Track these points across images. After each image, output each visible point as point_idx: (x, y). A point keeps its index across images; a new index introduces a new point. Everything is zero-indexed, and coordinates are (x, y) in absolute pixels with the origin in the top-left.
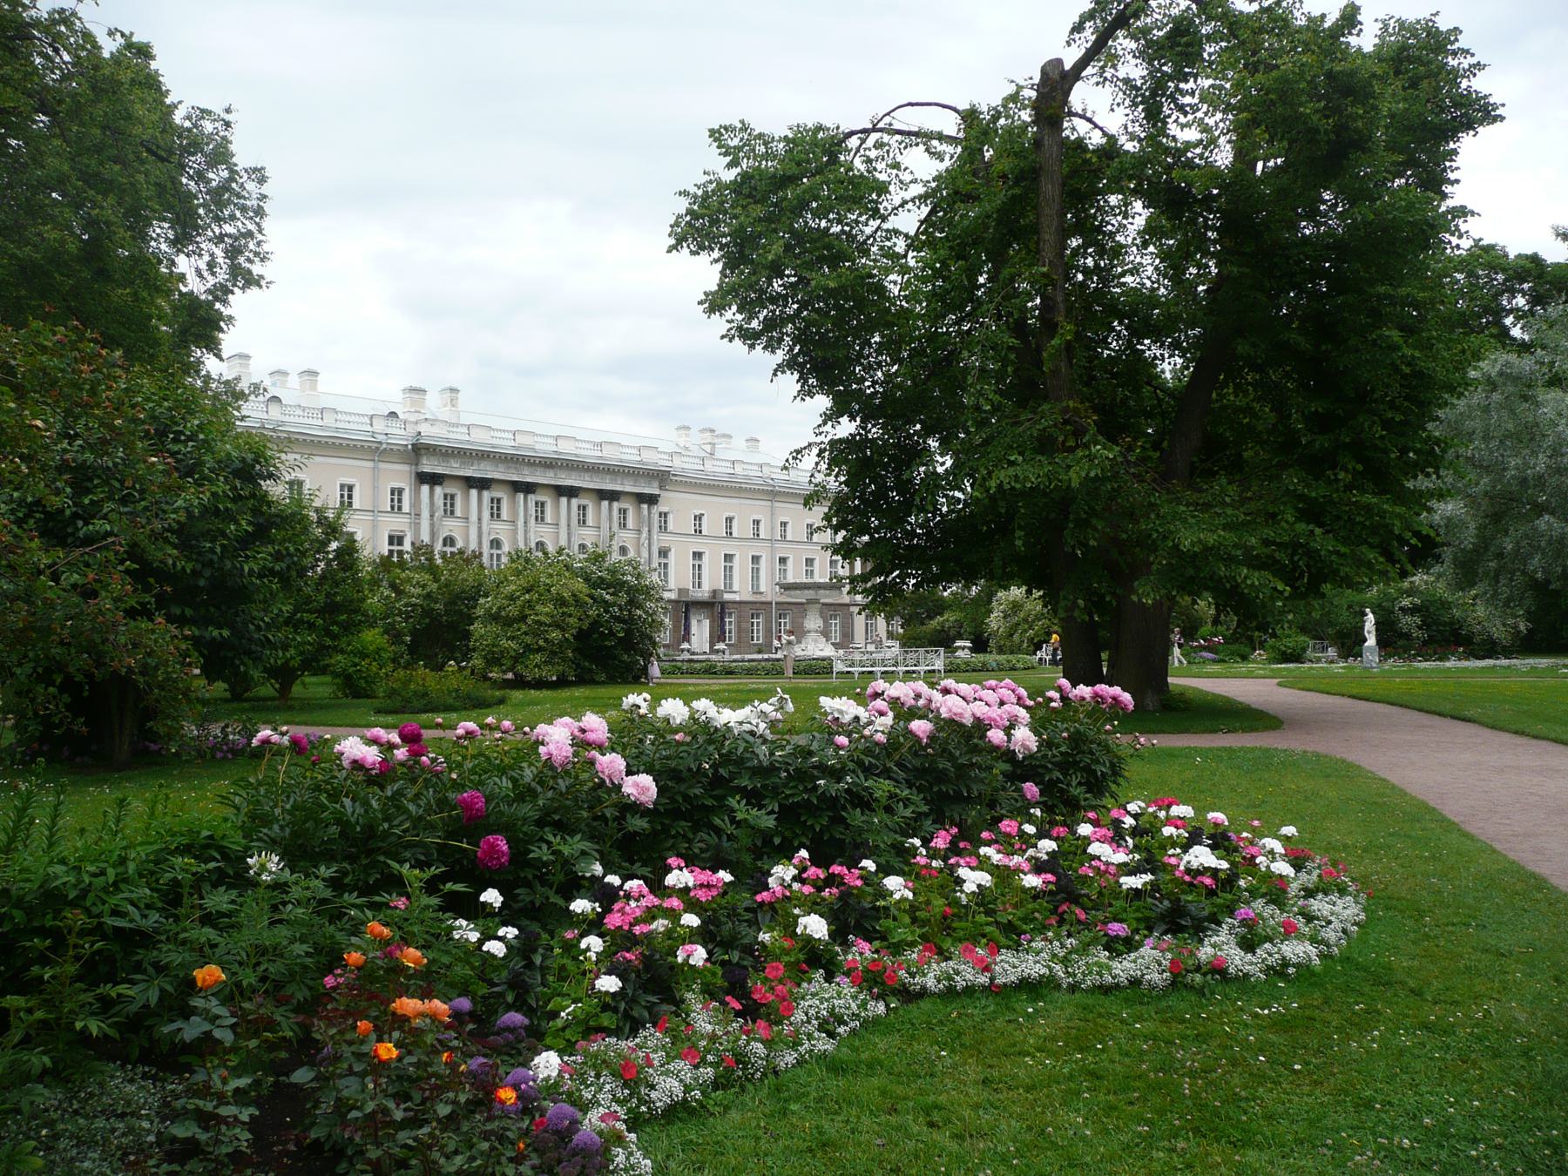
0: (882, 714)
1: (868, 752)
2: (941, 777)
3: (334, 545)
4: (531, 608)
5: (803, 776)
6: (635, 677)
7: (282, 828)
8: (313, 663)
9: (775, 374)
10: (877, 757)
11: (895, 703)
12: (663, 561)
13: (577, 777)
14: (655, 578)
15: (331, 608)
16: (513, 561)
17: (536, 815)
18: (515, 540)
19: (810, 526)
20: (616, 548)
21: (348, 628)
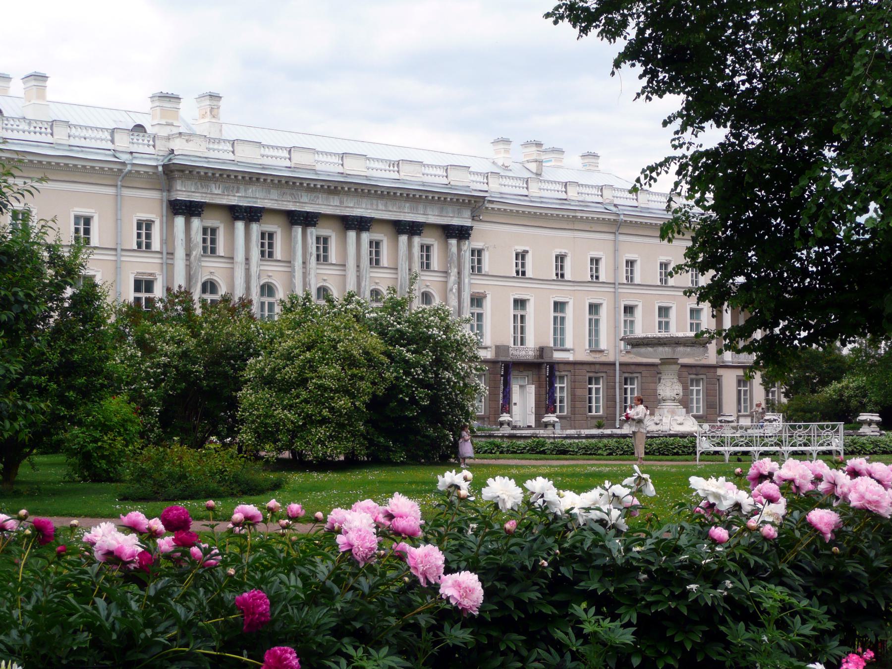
0: (771, 500)
1: (753, 548)
2: (851, 584)
3: (69, 292)
4: (313, 369)
5: (667, 579)
6: (448, 457)
7: (22, 634)
8: (44, 439)
9: (617, 64)
10: (765, 557)
11: (788, 486)
12: (477, 310)
13: (383, 575)
14: (466, 331)
15: (67, 369)
16: (288, 310)
17: (333, 622)
18: (291, 285)
19: (664, 265)
20: (417, 294)
21: (86, 393)
